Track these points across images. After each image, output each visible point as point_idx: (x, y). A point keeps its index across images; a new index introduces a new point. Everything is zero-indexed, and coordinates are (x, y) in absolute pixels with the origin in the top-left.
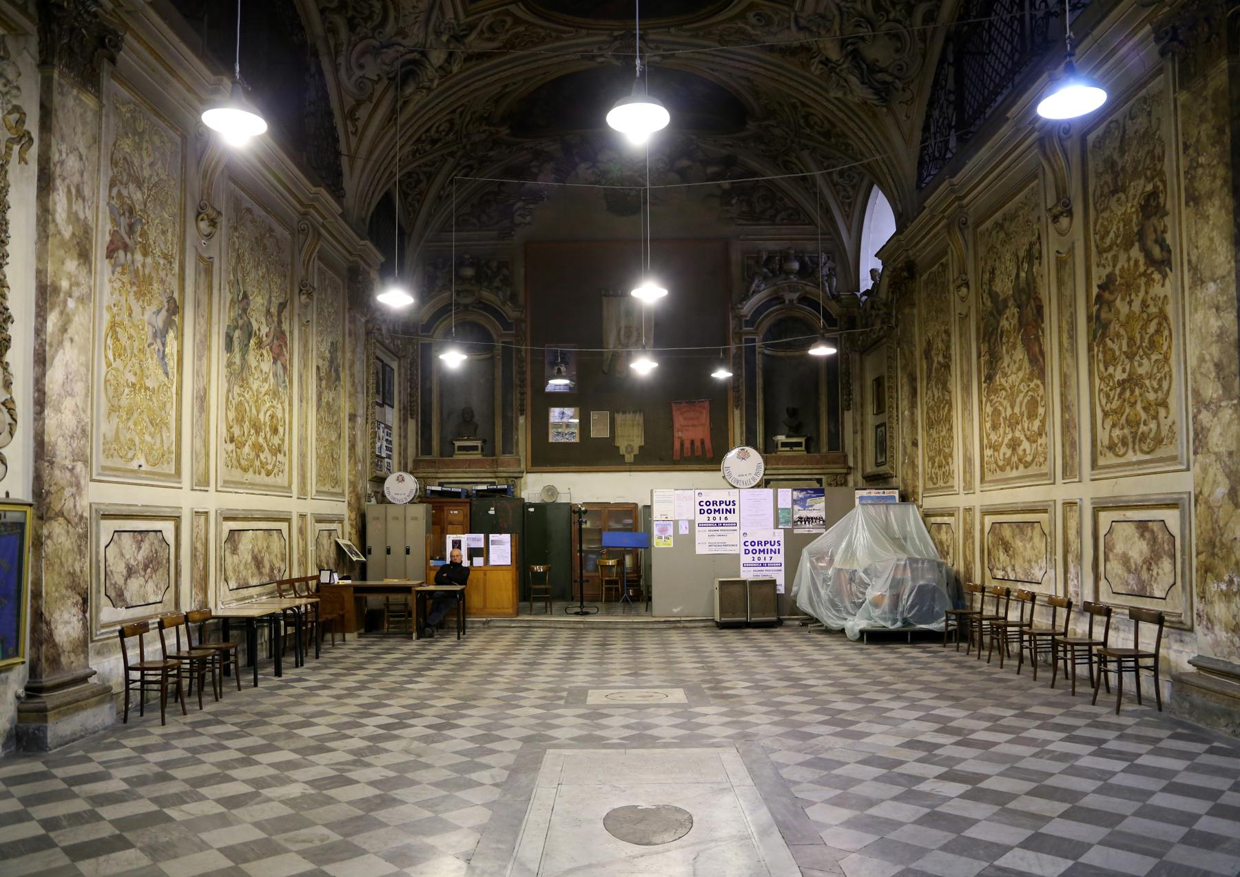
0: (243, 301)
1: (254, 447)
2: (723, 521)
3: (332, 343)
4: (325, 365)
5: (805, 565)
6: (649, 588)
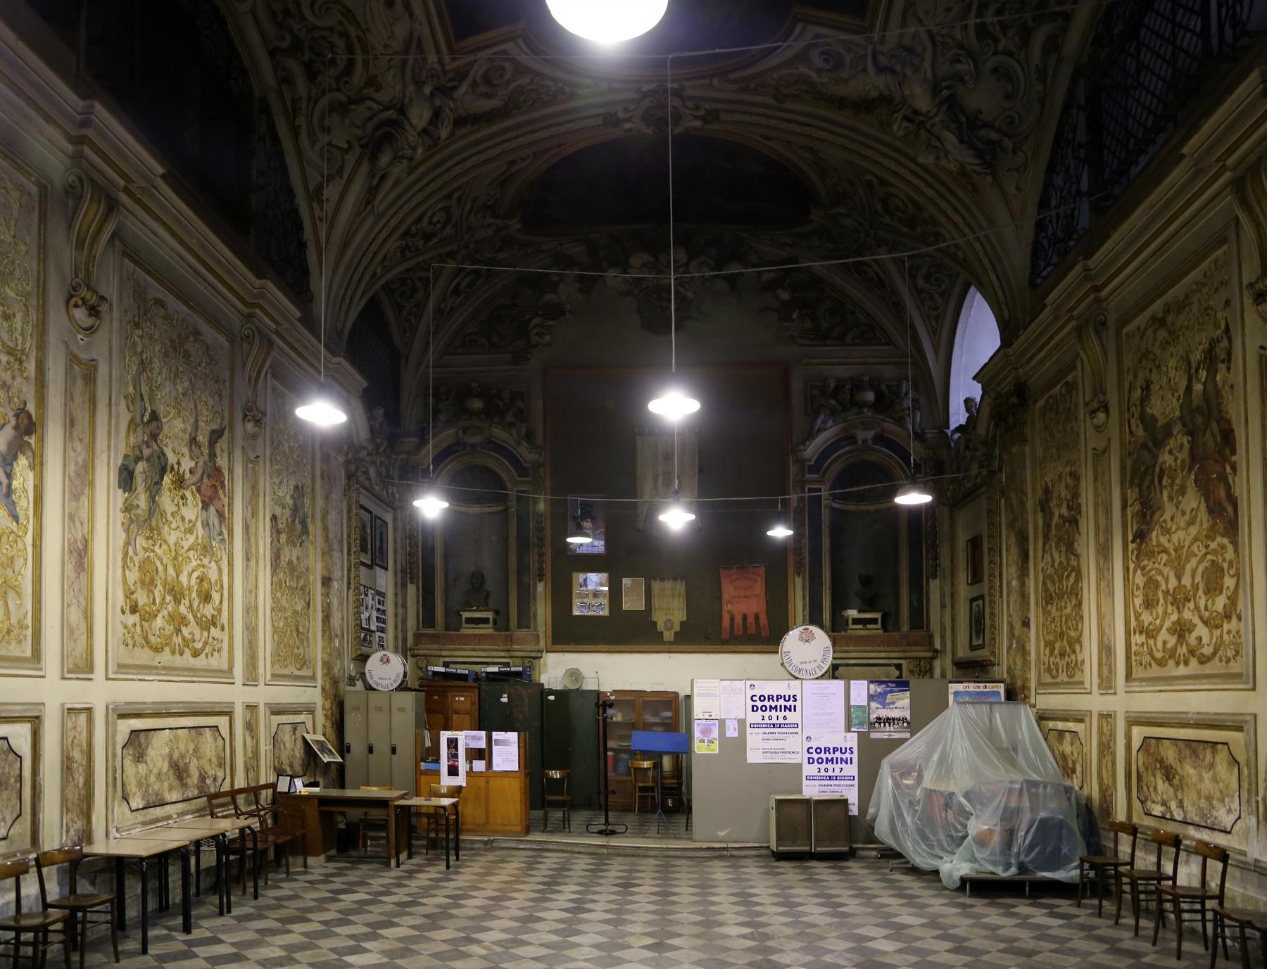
0: (153, 423)
1: (169, 619)
2: (781, 721)
3: (296, 487)
4: (284, 515)
5: (886, 781)
6: (689, 801)
